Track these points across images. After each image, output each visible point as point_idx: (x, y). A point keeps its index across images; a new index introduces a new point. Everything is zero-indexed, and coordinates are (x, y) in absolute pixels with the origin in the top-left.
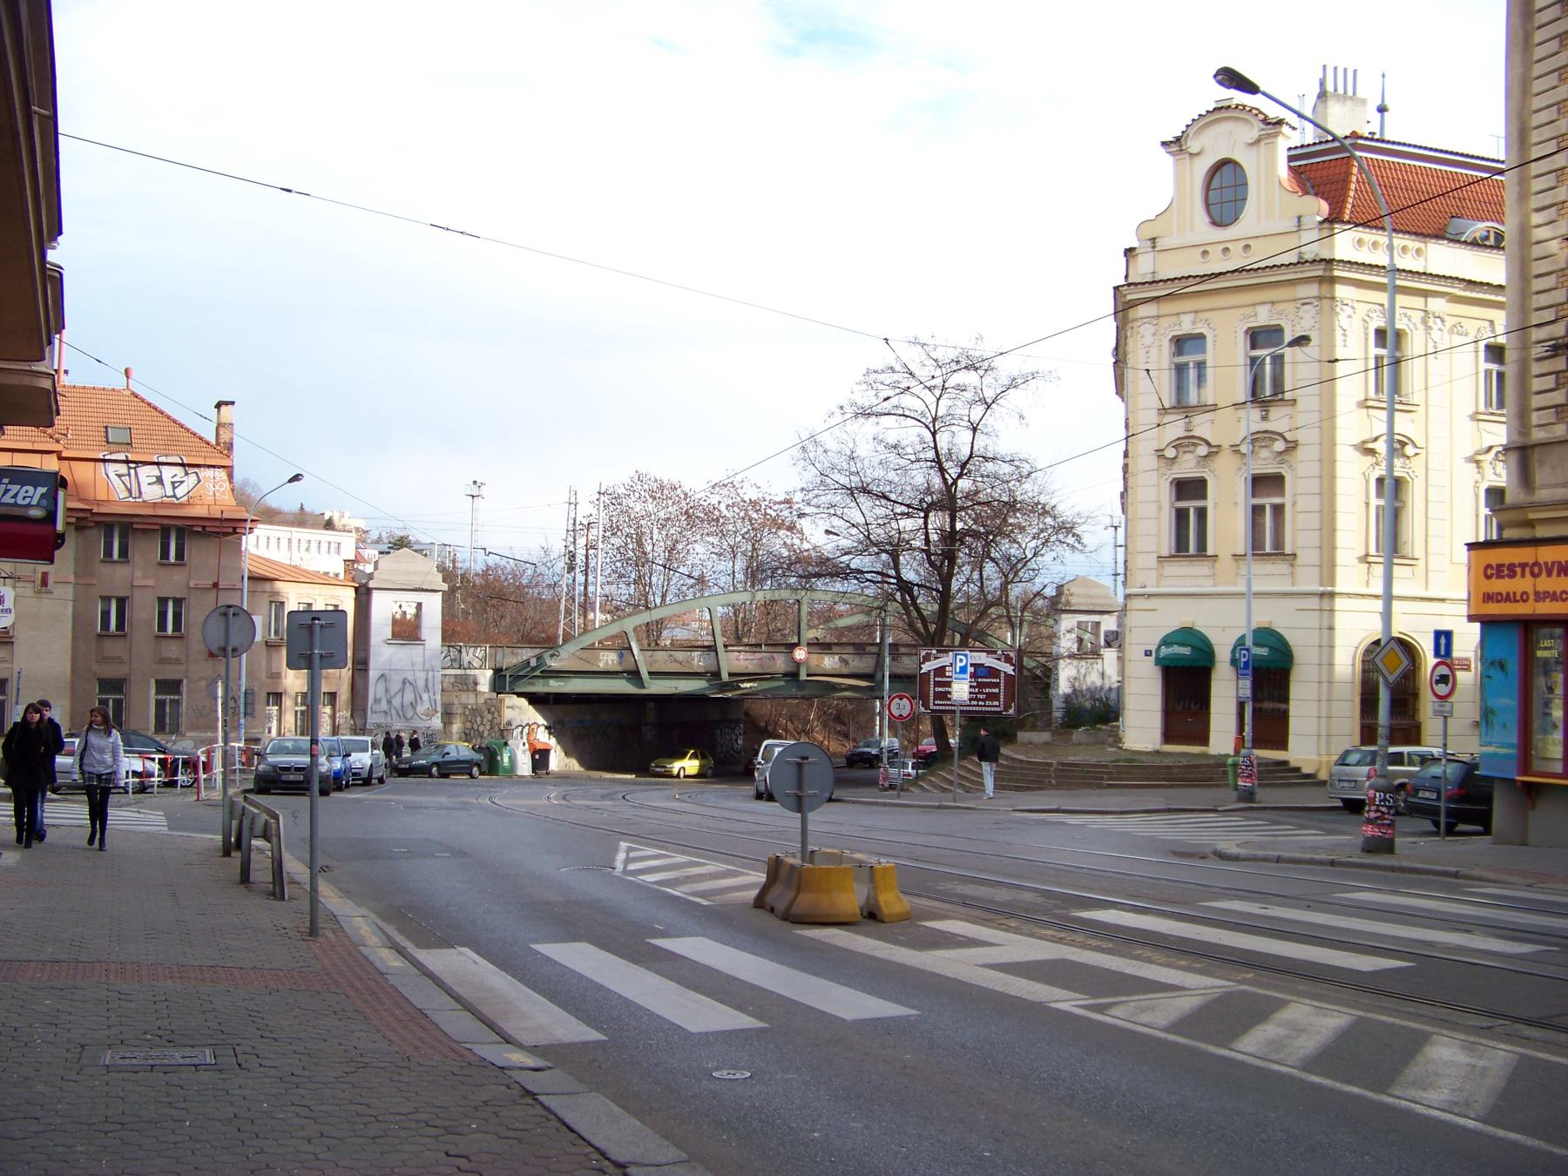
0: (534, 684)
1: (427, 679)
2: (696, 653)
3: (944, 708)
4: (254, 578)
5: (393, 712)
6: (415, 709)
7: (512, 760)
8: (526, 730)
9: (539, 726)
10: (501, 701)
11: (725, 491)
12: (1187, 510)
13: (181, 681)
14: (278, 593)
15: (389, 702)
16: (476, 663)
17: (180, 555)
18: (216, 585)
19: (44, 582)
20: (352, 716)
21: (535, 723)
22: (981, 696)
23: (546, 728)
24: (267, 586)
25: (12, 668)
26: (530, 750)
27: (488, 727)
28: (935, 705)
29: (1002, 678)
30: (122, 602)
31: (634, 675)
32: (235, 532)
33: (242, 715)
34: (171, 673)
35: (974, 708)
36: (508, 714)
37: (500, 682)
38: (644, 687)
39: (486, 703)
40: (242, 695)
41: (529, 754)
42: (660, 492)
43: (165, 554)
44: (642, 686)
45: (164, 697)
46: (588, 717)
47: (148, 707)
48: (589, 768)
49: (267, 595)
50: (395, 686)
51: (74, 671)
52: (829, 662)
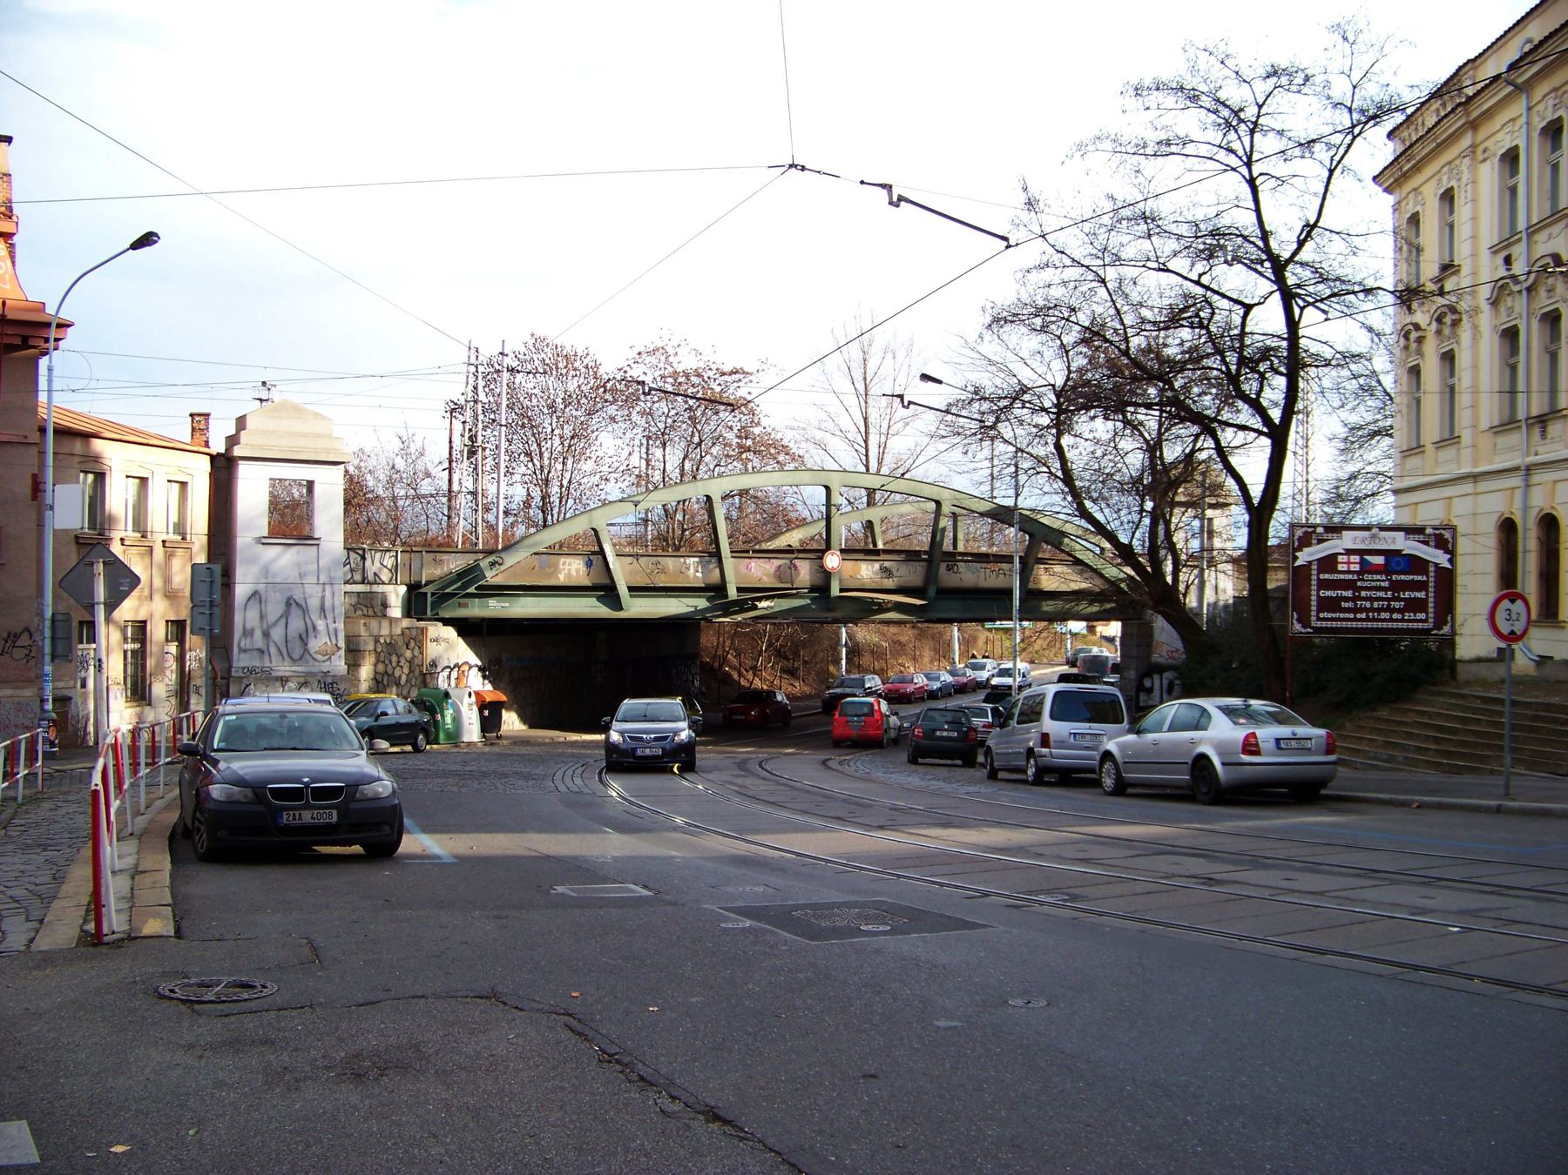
0: (466, 605)
1: (323, 598)
2: (692, 560)
3: (1334, 624)
4: (63, 433)
5: (273, 650)
6: (306, 644)
7: (457, 719)
8: (454, 674)
9: (470, 667)
10: (423, 631)
11: (652, 360)
14: (96, 459)
15: (266, 635)
16: (385, 576)
21: (466, 663)
22: (1397, 605)
23: (480, 669)
24: (78, 446)
26: (477, 702)
27: (406, 670)
28: (1319, 619)
29: (1431, 574)
31: (607, 591)
32: (25, 345)
33: (48, 658)
35: (1385, 625)
36: (432, 650)
37: (416, 603)
39: (403, 634)
40: (48, 623)
41: (475, 708)
42: (562, 362)
44: (619, 607)
48: (531, 727)
50: (274, 610)
52: (867, 572)
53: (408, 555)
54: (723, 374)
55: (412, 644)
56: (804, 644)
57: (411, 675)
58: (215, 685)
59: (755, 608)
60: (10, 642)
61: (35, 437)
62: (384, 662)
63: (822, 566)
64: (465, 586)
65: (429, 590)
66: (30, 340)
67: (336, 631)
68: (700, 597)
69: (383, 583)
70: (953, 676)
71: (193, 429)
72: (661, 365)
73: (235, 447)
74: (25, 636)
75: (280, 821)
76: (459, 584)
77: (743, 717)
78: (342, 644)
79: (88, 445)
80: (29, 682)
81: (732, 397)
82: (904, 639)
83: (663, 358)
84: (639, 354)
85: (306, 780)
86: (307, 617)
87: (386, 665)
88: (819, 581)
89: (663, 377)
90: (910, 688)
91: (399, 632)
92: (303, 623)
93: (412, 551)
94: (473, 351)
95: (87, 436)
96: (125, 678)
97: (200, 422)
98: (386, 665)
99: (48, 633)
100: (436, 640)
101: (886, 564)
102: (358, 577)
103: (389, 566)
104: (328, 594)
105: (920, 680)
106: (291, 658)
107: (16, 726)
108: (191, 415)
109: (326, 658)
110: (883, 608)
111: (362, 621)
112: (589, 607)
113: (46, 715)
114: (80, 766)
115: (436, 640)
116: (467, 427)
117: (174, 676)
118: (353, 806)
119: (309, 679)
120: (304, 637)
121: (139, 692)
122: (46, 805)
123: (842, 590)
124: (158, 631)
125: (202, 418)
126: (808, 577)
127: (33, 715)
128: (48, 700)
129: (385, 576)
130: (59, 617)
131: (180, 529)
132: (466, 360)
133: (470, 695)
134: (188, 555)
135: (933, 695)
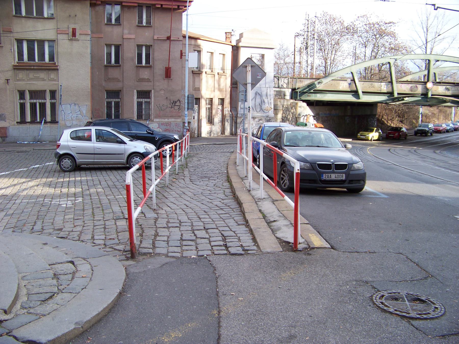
0: (310, 96)
1: (267, 92)
6: (261, 107)
8: (305, 118)
10: (297, 104)
11: (362, 19)
12: (35, 104)
13: (151, 91)
14: (199, 46)
16: (285, 86)
17: (148, 22)
18: (169, 38)
19: (74, 34)
20: (231, 111)
21: (309, 114)
23: (314, 117)
25: (58, 84)
27: (291, 116)
30: (118, 48)
31: (355, 93)
32: (179, 9)
33: (186, 109)
34: (145, 87)
36: (299, 110)
37: (295, 94)
38: (359, 99)
40: (186, 98)
42: (332, 20)
43: (141, 21)
45: (141, 100)
46: (328, 112)
47: (133, 106)
49: (193, 46)
51: (92, 86)
53: (292, 79)
54: (386, 24)
55: (293, 108)
56: (406, 112)
57: (293, 118)
58: (233, 119)
59: (403, 100)
60: (174, 104)
61: (181, 38)
62: (285, 113)
63: (426, 87)
64: (310, 90)
65: (298, 91)
66: (180, 6)
67: (271, 103)
68: (385, 96)
69: (284, 88)
70: (454, 125)
71: (226, 38)
72: (365, 21)
73: (240, 43)
74: (178, 102)
75: (322, 178)
76: (308, 89)
77: (393, 136)
78: (272, 107)
79: (196, 41)
80: (180, 117)
81: (389, 31)
82: (435, 112)
83: (366, 19)
84: (358, 17)
85: (332, 161)
86: (262, 98)
87: (285, 114)
88: (424, 92)
89: (366, 25)
90: (441, 128)
91: (290, 104)
92: (260, 100)
93: (293, 78)
94: (307, 15)
95: (196, 39)
96: (206, 116)
97: (228, 35)
98: (285, 114)
99: (186, 101)
100: (300, 107)
101: (448, 87)
102: (277, 86)
103: (286, 83)
104: (268, 91)
105: (444, 126)
106: (256, 111)
107: (175, 131)
108: (226, 33)
109: (268, 111)
110: (445, 102)
111: (279, 100)
112: (349, 98)
113: (186, 128)
114: (197, 144)
115: (300, 107)
116: (305, 40)
117: (220, 116)
118: (351, 172)
119: (262, 118)
120: (261, 105)
121: (210, 121)
122: (195, 159)
123: (432, 95)
124: (216, 102)
125: (229, 34)
126: (421, 90)
127: (180, 127)
128: (186, 123)
129: (285, 86)
130: (190, 96)
131: (223, 69)
132: (305, 18)
133: (313, 125)
134: (225, 78)
135: (447, 131)
